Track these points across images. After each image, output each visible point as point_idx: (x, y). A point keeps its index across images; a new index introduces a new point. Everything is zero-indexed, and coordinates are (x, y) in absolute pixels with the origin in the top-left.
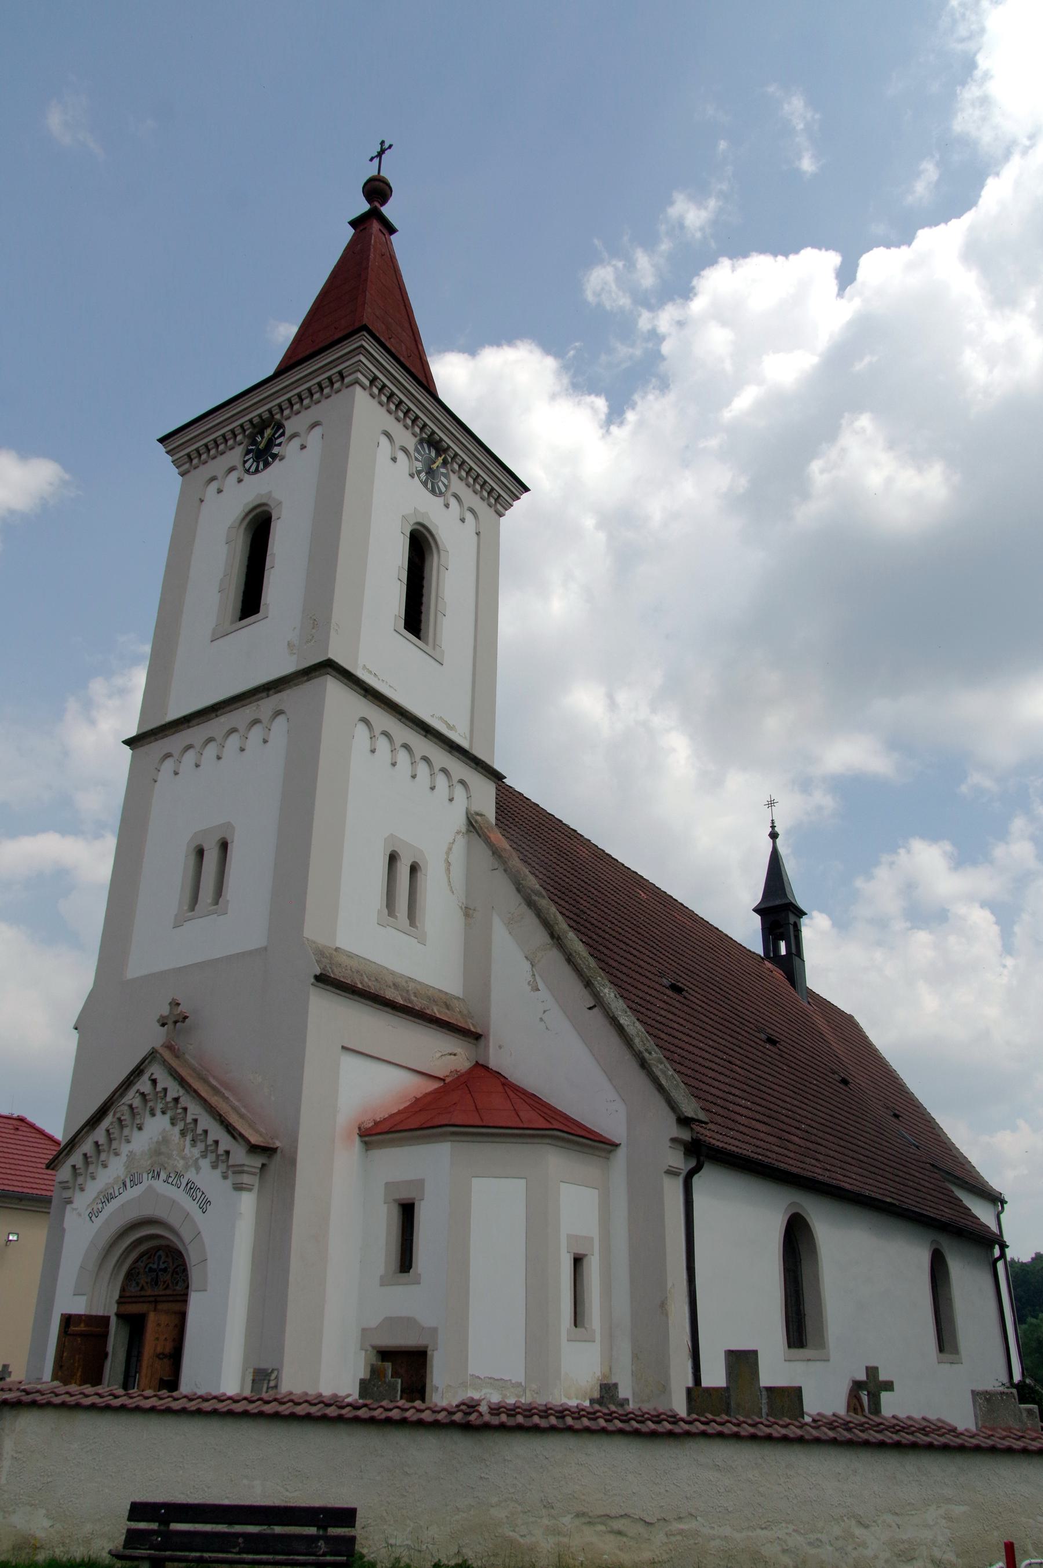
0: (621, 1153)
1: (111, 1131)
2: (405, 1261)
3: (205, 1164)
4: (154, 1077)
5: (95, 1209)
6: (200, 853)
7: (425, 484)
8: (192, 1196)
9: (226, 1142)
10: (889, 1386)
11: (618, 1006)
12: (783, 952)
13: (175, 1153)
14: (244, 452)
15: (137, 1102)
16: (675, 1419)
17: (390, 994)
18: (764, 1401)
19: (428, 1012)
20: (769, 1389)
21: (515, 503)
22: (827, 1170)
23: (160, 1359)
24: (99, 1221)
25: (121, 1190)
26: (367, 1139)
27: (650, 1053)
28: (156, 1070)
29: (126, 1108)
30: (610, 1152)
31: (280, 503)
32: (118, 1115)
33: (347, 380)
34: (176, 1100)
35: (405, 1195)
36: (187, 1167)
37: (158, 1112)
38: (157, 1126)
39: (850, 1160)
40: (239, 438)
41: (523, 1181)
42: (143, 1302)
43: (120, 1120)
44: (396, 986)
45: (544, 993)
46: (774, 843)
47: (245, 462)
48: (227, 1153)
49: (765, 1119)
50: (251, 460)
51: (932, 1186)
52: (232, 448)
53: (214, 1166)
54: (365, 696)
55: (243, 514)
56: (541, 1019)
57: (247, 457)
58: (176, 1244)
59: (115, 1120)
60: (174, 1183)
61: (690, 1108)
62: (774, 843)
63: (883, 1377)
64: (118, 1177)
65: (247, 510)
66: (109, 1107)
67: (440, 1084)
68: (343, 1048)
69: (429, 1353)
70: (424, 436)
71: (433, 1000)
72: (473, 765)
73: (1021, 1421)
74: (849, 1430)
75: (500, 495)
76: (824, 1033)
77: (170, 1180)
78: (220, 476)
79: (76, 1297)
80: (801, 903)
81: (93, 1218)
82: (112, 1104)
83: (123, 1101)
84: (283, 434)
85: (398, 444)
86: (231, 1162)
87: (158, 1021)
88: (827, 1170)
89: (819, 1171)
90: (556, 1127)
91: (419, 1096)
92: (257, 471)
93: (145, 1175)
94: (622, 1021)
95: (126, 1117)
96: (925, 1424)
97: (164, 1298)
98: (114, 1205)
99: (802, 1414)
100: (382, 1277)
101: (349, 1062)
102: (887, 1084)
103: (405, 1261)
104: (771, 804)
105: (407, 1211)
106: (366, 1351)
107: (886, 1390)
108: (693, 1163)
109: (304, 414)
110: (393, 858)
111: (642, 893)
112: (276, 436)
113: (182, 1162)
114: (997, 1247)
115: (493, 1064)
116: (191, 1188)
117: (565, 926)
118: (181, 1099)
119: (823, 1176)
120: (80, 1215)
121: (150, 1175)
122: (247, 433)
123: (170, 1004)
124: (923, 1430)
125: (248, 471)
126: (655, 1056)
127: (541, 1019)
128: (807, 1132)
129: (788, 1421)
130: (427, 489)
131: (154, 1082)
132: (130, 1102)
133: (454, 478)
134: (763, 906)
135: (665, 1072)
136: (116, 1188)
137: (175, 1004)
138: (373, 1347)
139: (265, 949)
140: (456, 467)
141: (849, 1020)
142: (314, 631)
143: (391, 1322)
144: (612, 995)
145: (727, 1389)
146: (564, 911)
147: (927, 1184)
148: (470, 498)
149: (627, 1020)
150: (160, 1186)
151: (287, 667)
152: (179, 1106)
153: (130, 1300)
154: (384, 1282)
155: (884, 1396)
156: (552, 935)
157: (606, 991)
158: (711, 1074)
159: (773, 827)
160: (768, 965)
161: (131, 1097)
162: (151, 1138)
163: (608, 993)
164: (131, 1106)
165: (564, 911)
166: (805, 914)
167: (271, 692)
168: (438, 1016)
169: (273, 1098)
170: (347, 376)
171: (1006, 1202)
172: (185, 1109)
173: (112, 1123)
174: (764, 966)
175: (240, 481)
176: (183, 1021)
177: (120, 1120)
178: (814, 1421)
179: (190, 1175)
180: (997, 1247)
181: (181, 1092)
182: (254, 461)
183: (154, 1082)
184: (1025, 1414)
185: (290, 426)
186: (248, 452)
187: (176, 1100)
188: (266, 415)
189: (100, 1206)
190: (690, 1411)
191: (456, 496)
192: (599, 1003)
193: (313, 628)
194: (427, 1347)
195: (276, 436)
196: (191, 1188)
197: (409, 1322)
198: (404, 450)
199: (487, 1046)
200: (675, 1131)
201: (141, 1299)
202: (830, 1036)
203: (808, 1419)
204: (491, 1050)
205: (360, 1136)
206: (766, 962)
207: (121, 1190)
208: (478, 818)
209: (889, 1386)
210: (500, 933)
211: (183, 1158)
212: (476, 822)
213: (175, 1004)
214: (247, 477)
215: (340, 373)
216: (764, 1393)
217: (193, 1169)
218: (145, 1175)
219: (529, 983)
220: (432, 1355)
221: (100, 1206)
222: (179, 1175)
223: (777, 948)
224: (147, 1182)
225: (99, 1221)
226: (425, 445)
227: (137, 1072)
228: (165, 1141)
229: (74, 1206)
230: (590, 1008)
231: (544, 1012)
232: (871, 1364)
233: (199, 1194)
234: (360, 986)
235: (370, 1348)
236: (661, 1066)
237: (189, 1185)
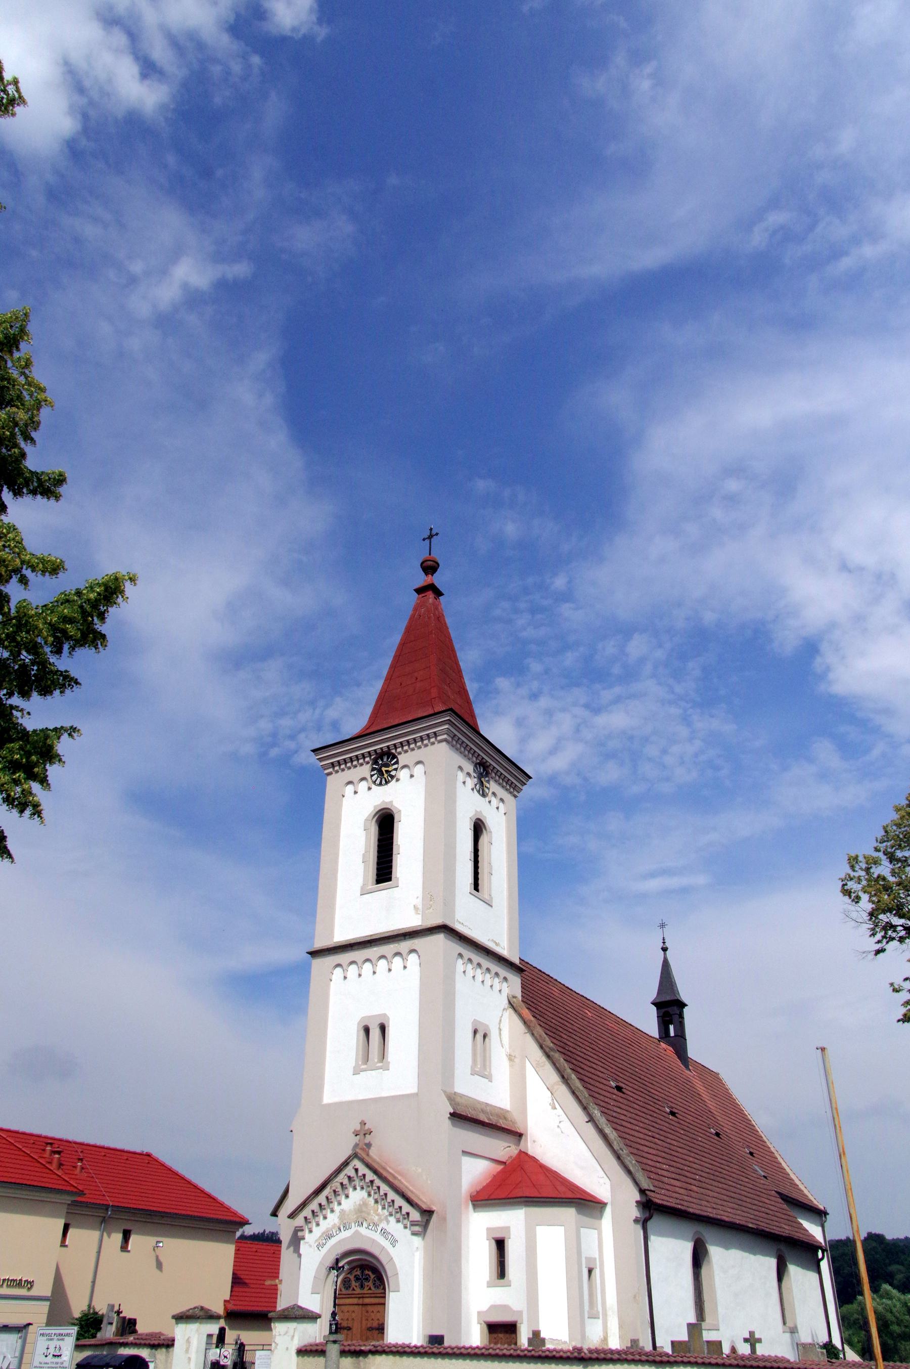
0: (608, 1210)
1: (330, 1197)
2: (501, 1272)
3: (392, 1220)
4: (356, 1167)
5: (321, 1243)
6: (367, 1030)
7: (479, 792)
8: (385, 1237)
9: (406, 1208)
10: (759, 1340)
11: (602, 1121)
12: (672, 1034)
13: (372, 1211)
14: (371, 769)
15: (346, 1181)
16: (667, 1355)
17: (483, 1118)
18: (706, 1347)
19: (499, 1124)
20: (708, 1342)
21: (524, 788)
22: (714, 1208)
23: (369, 1330)
24: (324, 1250)
25: (338, 1232)
26: (475, 1203)
27: (623, 1151)
28: (356, 1163)
29: (339, 1184)
30: (602, 1207)
31: (400, 811)
32: (334, 1188)
33: (439, 738)
34: (372, 1182)
35: (499, 1235)
36: (381, 1220)
37: (358, 1188)
38: (357, 1197)
39: (725, 1198)
40: (367, 759)
41: (563, 1227)
42: (355, 1298)
43: (335, 1191)
44: (483, 1111)
45: (559, 1111)
46: (665, 954)
47: (372, 776)
48: (408, 1214)
49: (677, 1177)
50: (376, 776)
51: (776, 1209)
52: (362, 765)
53: (398, 1221)
54: (460, 940)
55: (373, 814)
56: (558, 1126)
57: (373, 773)
58: (374, 1264)
59: (332, 1191)
60: (373, 1229)
61: (645, 1184)
62: (665, 954)
63: (757, 1336)
64: (335, 1224)
65: (376, 811)
66: (327, 1184)
67: (501, 1167)
68: (463, 1151)
69: (518, 1325)
70: (372, 757)
71: (498, 1116)
72: (510, 966)
73: (818, 1357)
74: (743, 1361)
75: (516, 785)
76: (701, 1093)
77: (370, 1227)
78: (355, 782)
79: (313, 1295)
80: (684, 998)
81: (320, 1248)
82: (330, 1181)
83: (336, 1180)
84: (397, 763)
85: (499, 797)
86: (411, 1219)
87: (353, 1133)
88: (714, 1208)
89: (710, 1210)
90: (578, 1197)
91: (495, 1174)
92: (381, 784)
93: (353, 1224)
94: (606, 1131)
95: (339, 1189)
96: (776, 1358)
97: (367, 1295)
98: (333, 1241)
99: (722, 1353)
100: (488, 1283)
101: (467, 1161)
102: (744, 1127)
103: (501, 1272)
104: (48, 1348)
105: (500, 1244)
106: (481, 1324)
107: (759, 1342)
108: (647, 1215)
109: (416, 751)
110: (475, 1032)
111: (588, 1013)
112: (392, 763)
113: (377, 1217)
114: (820, 1251)
115: (530, 1152)
116: (384, 1232)
117: (569, 1071)
118: (376, 1181)
119: (712, 1213)
120: (310, 1246)
121: (357, 1224)
122: (372, 757)
123: (360, 1123)
124: (775, 1361)
125: (374, 782)
126: (624, 1152)
127: (558, 1126)
128: (700, 1181)
129: (717, 1356)
130: (480, 794)
131: (356, 1170)
132: (341, 1181)
133: (492, 782)
134: (658, 1001)
135: (631, 1161)
136: (334, 1231)
137: (363, 1123)
138: (485, 1322)
139: (417, 1094)
140: (493, 775)
141: (716, 1076)
142: (431, 902)
143: (493, 1307)
144: (599, 1114)
145: (689, 1341)
146: (542, 1024)
147: (773, 1208)
148: (501, 792)
149: (608, 1130)
150: (363, 1230)
151: (414, 921)
152: (374, 1185)
153: (344, 1296)
154: (490, 1285)
155: (758, 1345)
156: (563, 1077)
157: (596, 1112)
158: (646, 1149)
159: (664, 939)
160: (663, 1045)
161: (342, 1177)
162: (355, 1202)
163: (597, 1113)
164: (342, 1184)
165: (542, 1024)
166: (687, 1005)
167: (407, 937)
168: (503, 1126)
169: (429, 1182)
170: (439, 736)
171: (828, 1214)
172: (379, 1188)
173: (330, 1193)
174: (660, 1047)
175: (369, 789)
176: (370, 1134)
177: (335, 1191)
178: (727, 1356)
179: (383, 1225)
180: (820, 1251)
181: (375, 1177)
182: (378, 777)
183: (356, 1170)
184: (820, 1354)
185: (403, 759)
186: (373, 769)
187: (372, 1182)
188: (385, 749)
189: (324, 1241)
190: (673, 1351)
191: (494, 794)
192: (591, 1119)
193: (431, 901)
194: (517, 1322)
195: (392, 763)
196: (384, 1232)
197: (505, 1308)
198: (468, 774)
199: (526, 1140)
200: (637, 1196)
201: (353, 1296)
202: (705, 1096)
203: (724, 1356)
204: (529, 1144)
205: (472, 1201)
206: (662, 1043)
207: (338, 1232)
208: (514, 999)
209: (759, 1340)
210: (530, 1071)
211: (378, 1215)
212: (514, 1002)
213: (363, 1123)
214: (373, 786)
215: (435, 733)
216: (705, 1343)
217: (385, 1222)
218: (353, 1224)
219: (550, 1104)
220: (520, 1327)
221: (324, 1241)
222: (376, 1225)
223: (667, 1031)
224: (354, 1228)
225: (324, 1250)
226: (478, 766)
227: (346, 1164)
228: (365, 1204)
229: (306, 1240)
230: (587, 1122)
231: (560, 1122)
232: (751, 1330)
233: (390, 1237)
234: (469, 1116)
235: (483, 1323)
236: (629, 1158)
237: (383, 1231)
